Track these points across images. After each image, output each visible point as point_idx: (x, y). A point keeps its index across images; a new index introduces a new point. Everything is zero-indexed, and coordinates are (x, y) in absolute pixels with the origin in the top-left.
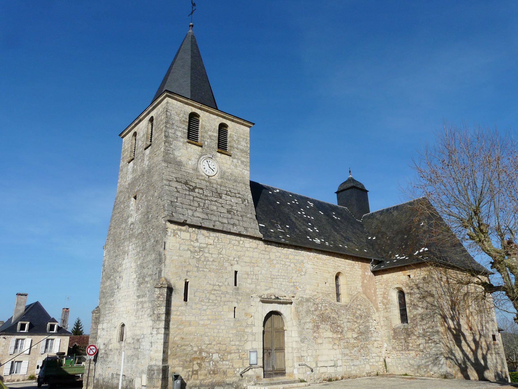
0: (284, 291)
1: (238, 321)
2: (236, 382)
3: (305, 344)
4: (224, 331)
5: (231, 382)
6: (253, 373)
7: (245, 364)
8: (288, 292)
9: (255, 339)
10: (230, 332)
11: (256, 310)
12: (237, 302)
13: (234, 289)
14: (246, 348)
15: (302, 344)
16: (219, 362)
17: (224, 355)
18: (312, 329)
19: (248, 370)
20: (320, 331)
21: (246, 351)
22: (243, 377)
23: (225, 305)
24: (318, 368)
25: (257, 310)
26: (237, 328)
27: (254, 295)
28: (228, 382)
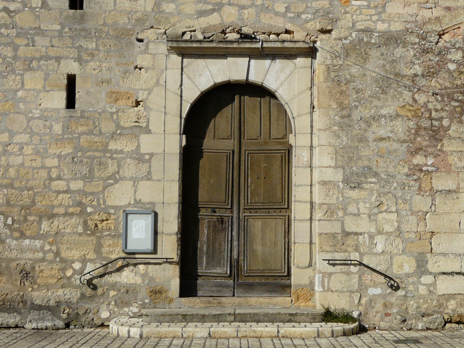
0: (284, 15)
1: (82, 117)
2: (69, 304)
3: (363, 194)
4: (28, 150)
5: (52, 303)
6: (139, 280)
7: (105, 250)
8: (304, 16)
9: (149, 173)
10: (51, 151)
11: (158, 81)
12: (79, 60)
13: (67, 17)
14: (110, 203)
15: (354, 194)
16: (8, 241)
17: (26, 220)
18: (404, 142)
19: (120, 269)
20: (445, 149)
21: (112, 211)
22: (100, 291)
23: (30, 69)
24: (427, 279)
25: (162, 82)
26: (79, 138)
27: (148, 35)
28: (38, 302)
